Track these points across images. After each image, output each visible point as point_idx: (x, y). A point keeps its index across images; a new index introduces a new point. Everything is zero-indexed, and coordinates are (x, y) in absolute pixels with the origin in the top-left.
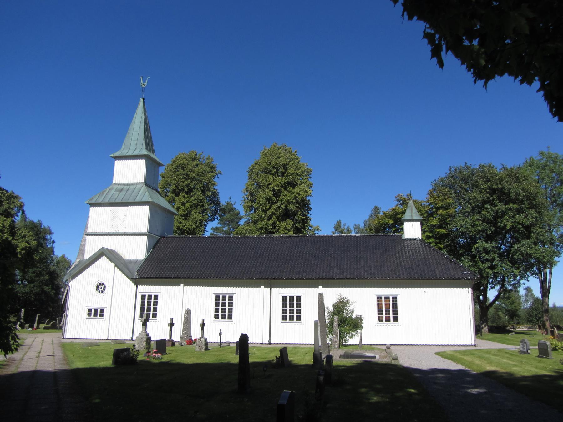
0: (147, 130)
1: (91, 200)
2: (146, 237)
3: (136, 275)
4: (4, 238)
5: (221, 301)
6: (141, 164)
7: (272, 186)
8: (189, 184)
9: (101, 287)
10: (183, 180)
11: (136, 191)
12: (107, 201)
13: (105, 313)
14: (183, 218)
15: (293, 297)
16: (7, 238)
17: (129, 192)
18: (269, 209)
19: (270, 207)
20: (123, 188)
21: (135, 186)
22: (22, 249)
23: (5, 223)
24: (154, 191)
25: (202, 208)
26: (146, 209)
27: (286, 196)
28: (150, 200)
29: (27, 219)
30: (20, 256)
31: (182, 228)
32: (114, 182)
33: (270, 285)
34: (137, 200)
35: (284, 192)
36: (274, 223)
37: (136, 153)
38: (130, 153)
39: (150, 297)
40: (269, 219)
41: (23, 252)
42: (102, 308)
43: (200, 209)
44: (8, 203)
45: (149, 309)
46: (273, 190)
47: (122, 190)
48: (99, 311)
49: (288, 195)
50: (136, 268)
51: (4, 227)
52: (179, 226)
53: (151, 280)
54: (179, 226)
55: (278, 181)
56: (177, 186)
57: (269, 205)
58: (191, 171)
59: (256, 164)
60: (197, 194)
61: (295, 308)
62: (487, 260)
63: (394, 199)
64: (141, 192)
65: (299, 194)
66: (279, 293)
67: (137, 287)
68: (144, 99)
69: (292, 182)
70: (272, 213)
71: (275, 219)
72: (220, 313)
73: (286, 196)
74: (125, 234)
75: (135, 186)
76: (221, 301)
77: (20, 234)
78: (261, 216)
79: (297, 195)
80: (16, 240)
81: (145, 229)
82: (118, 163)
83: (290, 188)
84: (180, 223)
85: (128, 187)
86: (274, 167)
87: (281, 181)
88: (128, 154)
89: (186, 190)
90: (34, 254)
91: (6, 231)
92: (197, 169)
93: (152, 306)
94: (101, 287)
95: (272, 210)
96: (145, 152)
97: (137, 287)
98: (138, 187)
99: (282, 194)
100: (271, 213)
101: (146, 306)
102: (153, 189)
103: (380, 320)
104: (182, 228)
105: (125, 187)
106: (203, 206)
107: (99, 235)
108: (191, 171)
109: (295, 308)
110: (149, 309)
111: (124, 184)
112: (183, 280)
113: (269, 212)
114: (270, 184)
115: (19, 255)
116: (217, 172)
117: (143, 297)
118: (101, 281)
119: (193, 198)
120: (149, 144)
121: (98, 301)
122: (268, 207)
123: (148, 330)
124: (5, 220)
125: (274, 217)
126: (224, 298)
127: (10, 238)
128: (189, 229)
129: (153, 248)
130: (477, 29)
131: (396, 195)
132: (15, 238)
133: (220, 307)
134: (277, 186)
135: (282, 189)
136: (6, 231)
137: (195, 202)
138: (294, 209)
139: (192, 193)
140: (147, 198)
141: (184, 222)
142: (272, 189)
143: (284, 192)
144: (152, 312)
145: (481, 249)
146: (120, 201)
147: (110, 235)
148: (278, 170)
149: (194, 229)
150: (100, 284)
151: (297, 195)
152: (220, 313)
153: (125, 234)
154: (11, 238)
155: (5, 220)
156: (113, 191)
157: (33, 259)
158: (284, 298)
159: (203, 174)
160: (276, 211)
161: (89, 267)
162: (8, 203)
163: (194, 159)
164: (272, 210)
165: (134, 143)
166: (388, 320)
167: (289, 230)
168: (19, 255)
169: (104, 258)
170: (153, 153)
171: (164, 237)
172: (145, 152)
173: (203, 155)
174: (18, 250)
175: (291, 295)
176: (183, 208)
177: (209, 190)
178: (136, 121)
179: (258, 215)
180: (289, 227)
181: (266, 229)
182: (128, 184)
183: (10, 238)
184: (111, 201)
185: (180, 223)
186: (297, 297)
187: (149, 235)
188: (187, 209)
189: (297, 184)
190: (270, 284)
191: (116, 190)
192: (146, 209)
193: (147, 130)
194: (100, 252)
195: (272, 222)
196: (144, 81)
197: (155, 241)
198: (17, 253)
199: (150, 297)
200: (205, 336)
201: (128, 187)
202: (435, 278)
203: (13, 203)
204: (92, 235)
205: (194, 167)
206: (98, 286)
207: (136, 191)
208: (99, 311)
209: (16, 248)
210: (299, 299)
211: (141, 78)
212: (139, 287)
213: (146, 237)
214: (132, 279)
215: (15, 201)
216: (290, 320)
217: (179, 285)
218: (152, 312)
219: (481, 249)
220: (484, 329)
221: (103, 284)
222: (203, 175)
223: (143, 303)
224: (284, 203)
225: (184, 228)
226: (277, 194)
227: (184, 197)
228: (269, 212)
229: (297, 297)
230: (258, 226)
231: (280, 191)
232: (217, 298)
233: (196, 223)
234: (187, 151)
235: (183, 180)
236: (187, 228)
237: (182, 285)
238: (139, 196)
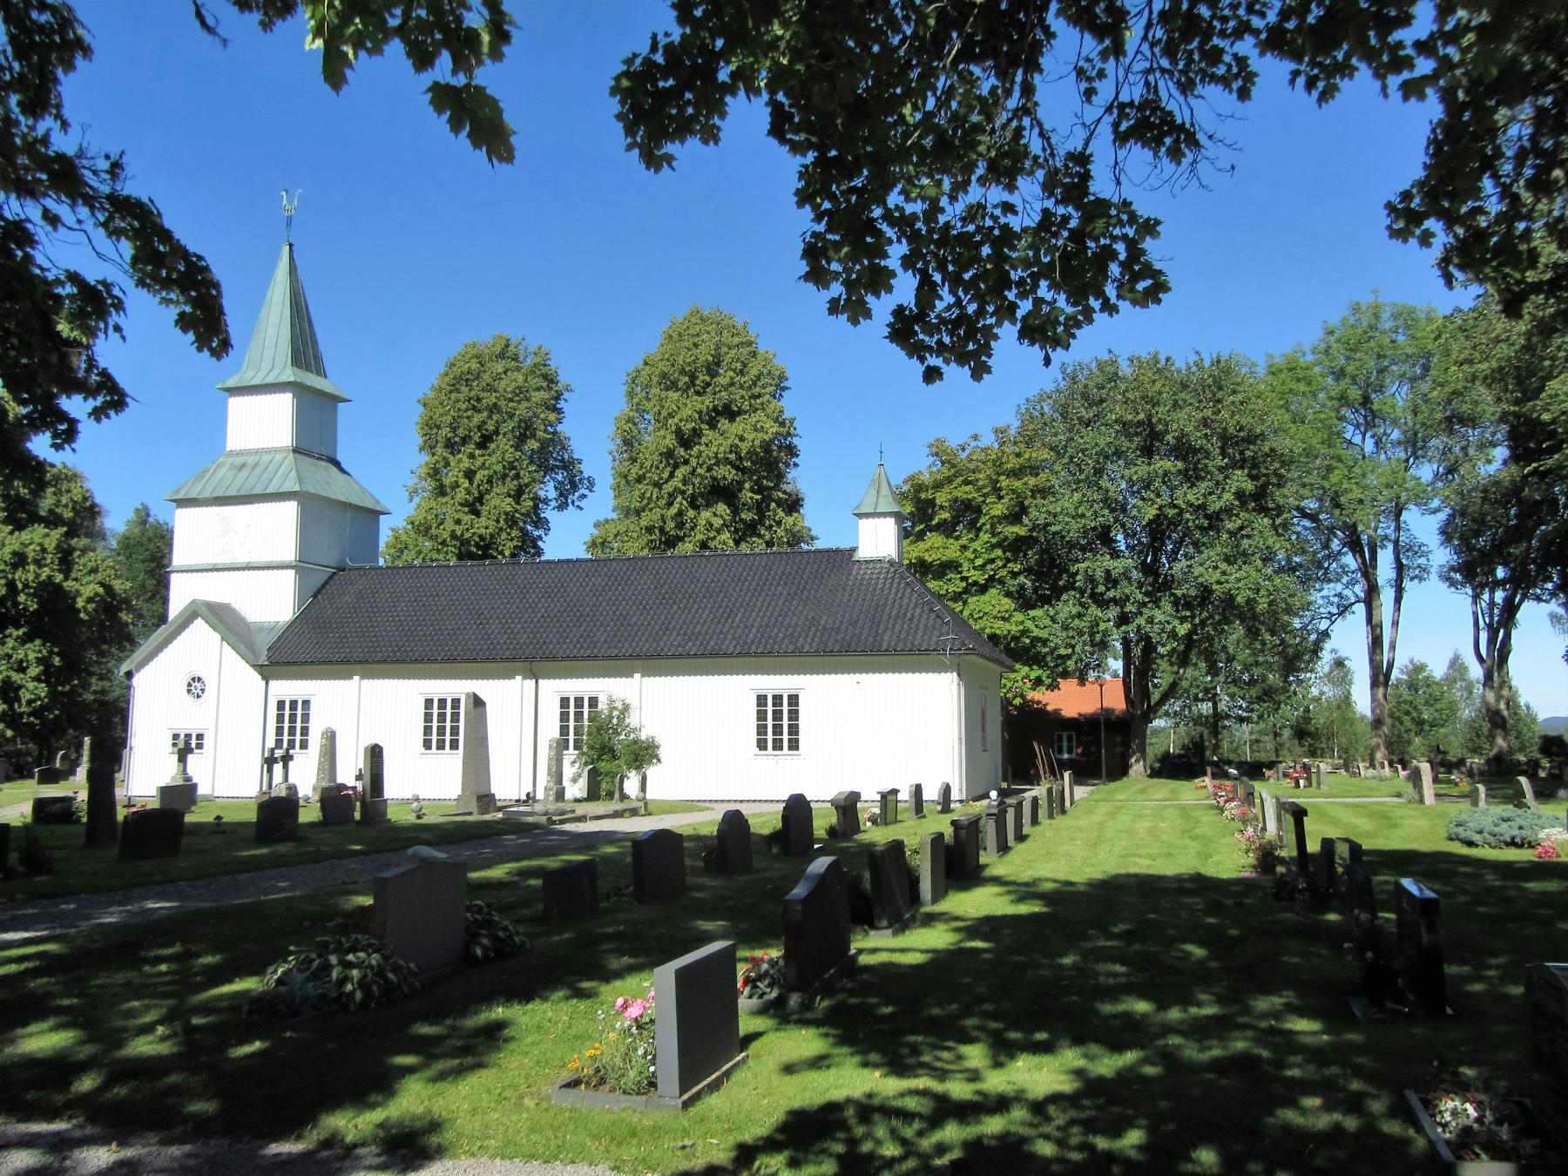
0: (301, 319)
1: (178, 491)
2: (293, 572)
3: (263, 660)
4: (43, 577)
5: (572, 710)
6: (282, 406)
7: (676, 420)
8: (484, 423)
9: (195, 686)
10: (469, 413)
11: (272, 467)
12: (207, 494)
13: (205, 742)
14: (466, 509)
15: (781, 697)
16: (50, 577)
17: (257, 471)
18: (667, 481)
19: (672, 475)
20: (247, 461)
21: (270, 457)
22: (90, 600)
23: (46, 542)
24: (323, 463)
25: (516, 482)
26: (290, 509)
27: (716, 442)
28: (297, 488)
29: (151, 519)
30: (86, 618)
31: (462, 535)
32: (228, 449)
33: (535, 676)
34: (270, 490)
35: (709, 434)
36: (680, 513)
37: (270, 379)
38: (257, 381)
39: (456, 702)
40: (670, 504)
41: (91, 607)
42: (200, 732)
43: (512, 485)
44: (55, 494)
45: (292, 731)
46: (679, 433)
47: (243, 465)
48: (194, 737)
49: (720, 440)
50: (264, 642)
51: (44, 550)
52: (453, 531)
53: (328, 667)
54: (453, 531)
55: (689, 408)
56: (454, 430)
57: (669, 469)
58: (490, 388)
59: (646, 363)
60: (503, 447)
61: (770, 722)
62: (1114, 601)
63: (927, 451)
64: (281, 470)
65: (742, 439)
66: (554, 689)
67: (267, 683)
68: (291, 245)
69: (727, 407)
70: (676, 488)
71: (681, 504)
72: (434, 737)
73: (716, 442)
74: (249, 567)
75: (270, 457)
76: (572, 710)
77: (85, 565)
78: (650, 498)
79: (737, 441)
80: (76, 579)
81: (289, 553)
82: (236, 404)
83: (724, 423)
84: (458, 522)
85: (258, 458)
86: (683, 372)
87: (699, 406)
88: (254, 382)
89: (477, 438)
90: (120, 610)
91: (49, 561)
92: (503, 384)
93: (299, 725)
94: (195, 686)
95: (676, 482)
96: (289, 374)
97: (267, 683)
98: (279, 456)
99: (703, 440)
100: (671, 490)
101: (286, 725)
102: (318, 459)
103: (762, 745)
104: (462, 535)
105: (252, 460)
106: (517, 476)
107: (197, 571)
108: (490, 388)
109: (770, 722)
110: (292, 731)
111: (249, 452)
112: (358, 667)
113: (668, 488)
114: (671, 416)
115: (82, 615)
116: (560, 387)
117: (281, 705)
118: (198, 674)
119: (494, 459)
120: (305, 351)
121: (191, 718)
122: (666, 475)
123: (190, 771)
124: (47, 535)
125: (679, 499)
126: (778, 699)
127: (59, 577)
128: (481, 537)
129: (315, 596)
130: (985, 61)
131: (931, 440)
132: (73, 575)
133: (435, 724)
134: (689, 419)
135: (703, 426)
136: (49, 561)
137: (499, 468)
138: (730, 478)
139: (493, 446)
140: (291, 485)
141: (467, 518)
142: (673, 428)
143: (709, 434)
144: (298, 738)
145: (1099, 574)
146: (234, 494)
147: (218, 570)
148: (693, 377)
149: (492, 536)
150: (193, 679)
151: (737, 441)
152: (434, 737)
153: (249, 567)
154: (61, 576)
155: (47, 535)
156: (223, 470)
157: (119, 621)
158: (564, 702)
159: (517, 395)
160: (684, 485)
161: (166, 646)
162: (55, 494)
163: (502, 355)
164: (676, 482)
165: (268, 354)
166: (778, 746)
167: (719, 531)
168: (82, 615)
169: (199, 623)
170: (321, 372)
171: (344, 570)
172: (289, 374)
173: (525, 343)
174: (80, 603)
175: (579, 695)
176: (467, 485)
177: (533, 436)
178: (274, 300)
179: (642, 496)
180: (717, 522)
181: (662, 530)
182: (257, 452)
183: (59, 577)
184: (219, 493)
185: (458, 522)
186: (790, 697)
187: (301, 566)
188: (479, 486)
189: (740, 412)
190: (531, 670)
191: (232, 467)
192: (290, 509)
193: (301, 319)
194: (190, 612)
195: (675, 511)
196: (290, 201)
197: (319, 579)
198: (79, 611)
199: (442, 702)
200: (291, 780)
201: (258, 458)
202: (799, 652)
203: (68, 491)
204: (182, 571)
205: (498, 378)
206: (189, 685)
207: (272, 467)
208: (194, 737)
209: (74, 599)
210: (794, 700)
211: (284, 193)
212: (271, 683)
213: (293, 572)
214: (259, 668)
215: (72, 485)
216: (774, 748)
217: (350, 677)
218: (298, 738)
219: (1099, 574)
220: (1134, 768)
221: (199, 679)
222: (517, 398)
223: (280, 718)
224: (704, 462)
225: (467, 535)
226: (687, 440)
227: (472, 456)
228: (668, 488)
229: (790, 697)
230: (644, 523)
231: (697, 433)
232: (761, 700)
233: (498, 521)
234: (486, 336)
235: (469, 413)
236: (474, 534)
237: (356, 678)
238: (274, 481)
